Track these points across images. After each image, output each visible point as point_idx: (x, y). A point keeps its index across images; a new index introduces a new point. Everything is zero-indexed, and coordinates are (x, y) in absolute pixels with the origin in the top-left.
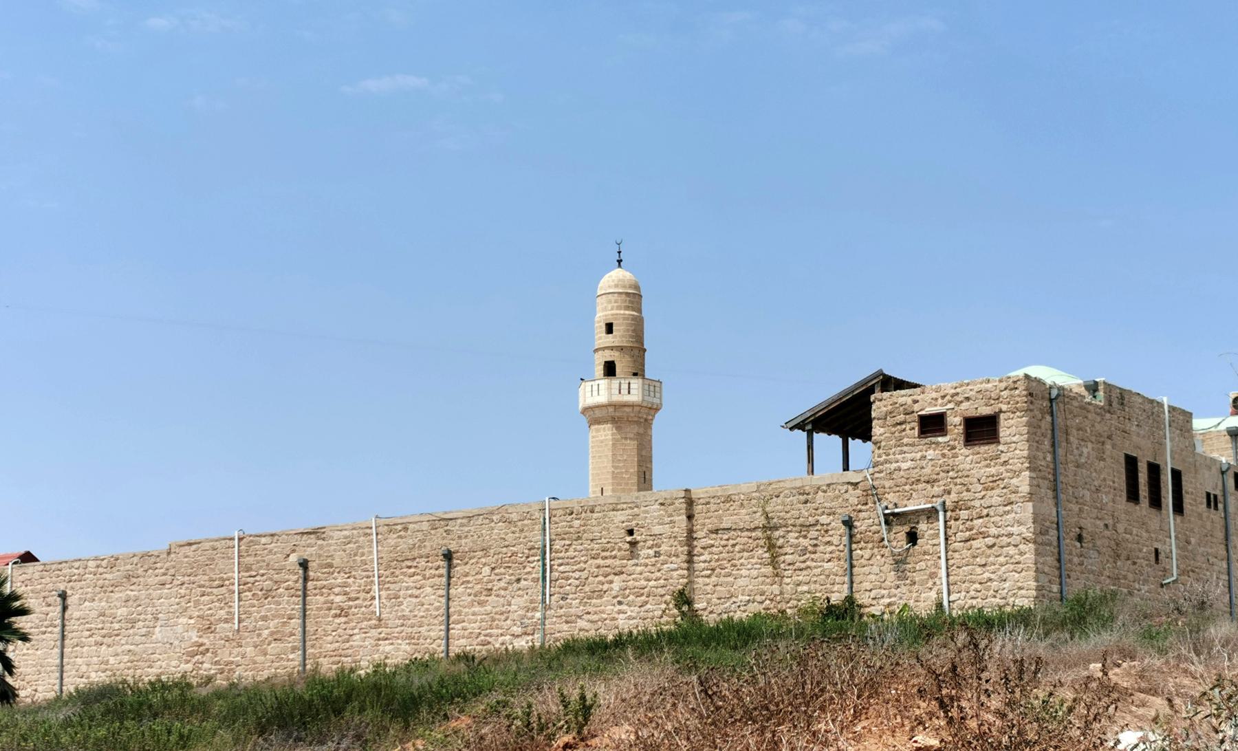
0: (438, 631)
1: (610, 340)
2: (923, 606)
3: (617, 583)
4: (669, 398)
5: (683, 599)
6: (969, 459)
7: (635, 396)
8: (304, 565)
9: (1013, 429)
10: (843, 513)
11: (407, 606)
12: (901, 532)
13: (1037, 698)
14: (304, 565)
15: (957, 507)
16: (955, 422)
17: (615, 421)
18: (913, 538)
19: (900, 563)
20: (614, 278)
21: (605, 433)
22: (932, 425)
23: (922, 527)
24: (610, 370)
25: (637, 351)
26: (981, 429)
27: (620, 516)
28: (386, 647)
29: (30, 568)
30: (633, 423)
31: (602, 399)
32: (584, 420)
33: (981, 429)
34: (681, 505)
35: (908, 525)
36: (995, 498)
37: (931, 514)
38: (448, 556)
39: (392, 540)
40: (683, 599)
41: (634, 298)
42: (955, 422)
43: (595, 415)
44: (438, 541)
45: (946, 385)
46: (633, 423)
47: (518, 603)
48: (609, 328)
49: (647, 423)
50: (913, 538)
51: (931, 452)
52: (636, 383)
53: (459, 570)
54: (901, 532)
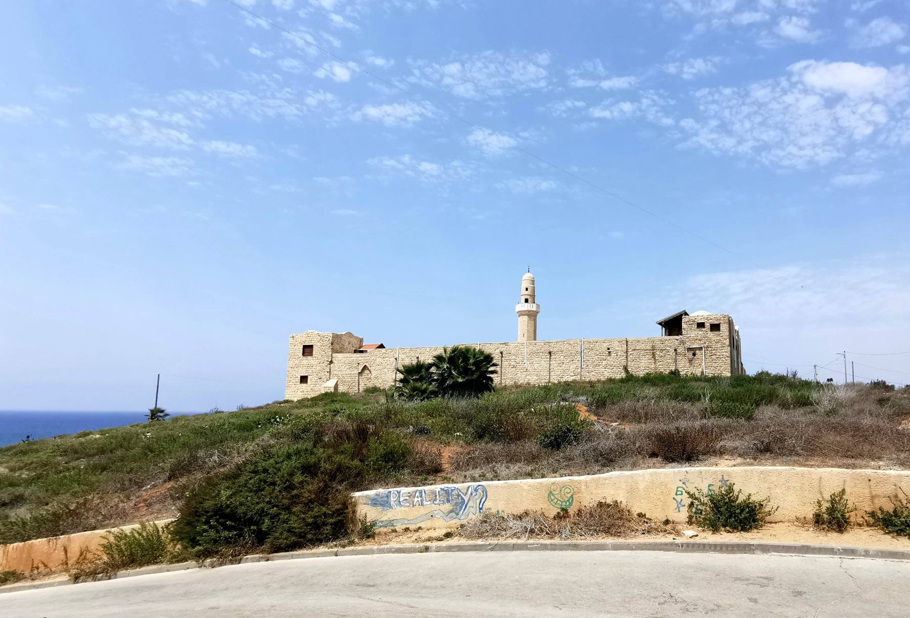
0: (546, 373)
1: (527, 292)
3: (604, 362)
5: (625, 368)
6: (711, 335)
7: (534, 309)
8: (502, 353)
9: (724, 328)
11: (536, 366)
12: (691, 353)
14: (502, 353)
15: (707, 347)
16: (707, 325)
17: (528, 315)
18: (694, 354)
19: (690, 361)
20: (527, 276)
21: (525, 318)
22: (701, 325)
24: (526, 301)
26: (715, 327)
27: (605, 345)
28: (529, 377)
29: (383, 350)
30: (532, 316)
31: (526, 309)
33: (715, 327)
35: (694, 351)
36: (719, 345)
37: (701, 349)
38: (550, 353)
39: (531, 347)
40: (625, 368)
41: (533, 282)
42: (707, 325)
43: (521, 313)
44: (547, 348)
45: (698, 313)
46: (532, 316)
47: (573, 367)
48: (527, 289)
49: (536, 316)
50: (694, 354)
51: (700, 333)
54: (691, 353)
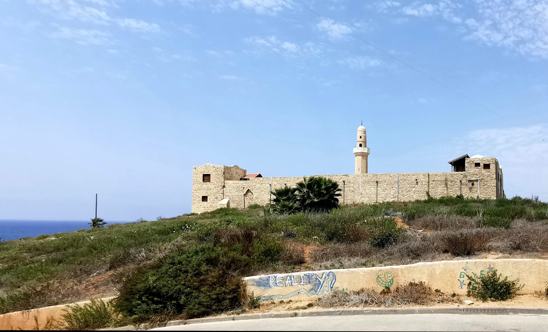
0: (375, 196)
2: (475, 196)
3: (414, 189)
4: (371, 152)
5: (428, 193)
6: (484, 171)
7: (366, 151)
10: (460, 179)
12: (471, 183)
13: (111, 309)
14: (344, 182)
15: (481, 180)
16: (482, 164)
17: (362, 155)
18: (473, 184)
19: (470, 189)
20: (361, 128)
21: (360, 158)
22: (477, 165)
23: (475, 183)
24: (361, 145)
25: (365, 142)
26: (487, 166)
29: (261, 179)
30: (365, 156)
31: (360, 151)
32: (354, 155)
33: (487, 166)
34: (427, 175)
35: (472, 182)
37: (477, 181)
38: (377, 182)
39: (364, 178)
40: (428, 193)
42: (482, 164)
43: (357, 154)
44: (375, 179)
46: (365, 156)
47: (393, 192)
48: (361, 137)
50: (473, 184)
51: (477, 170)
52: (366, 149)
53: (379, 185)
54: (471, 183)
